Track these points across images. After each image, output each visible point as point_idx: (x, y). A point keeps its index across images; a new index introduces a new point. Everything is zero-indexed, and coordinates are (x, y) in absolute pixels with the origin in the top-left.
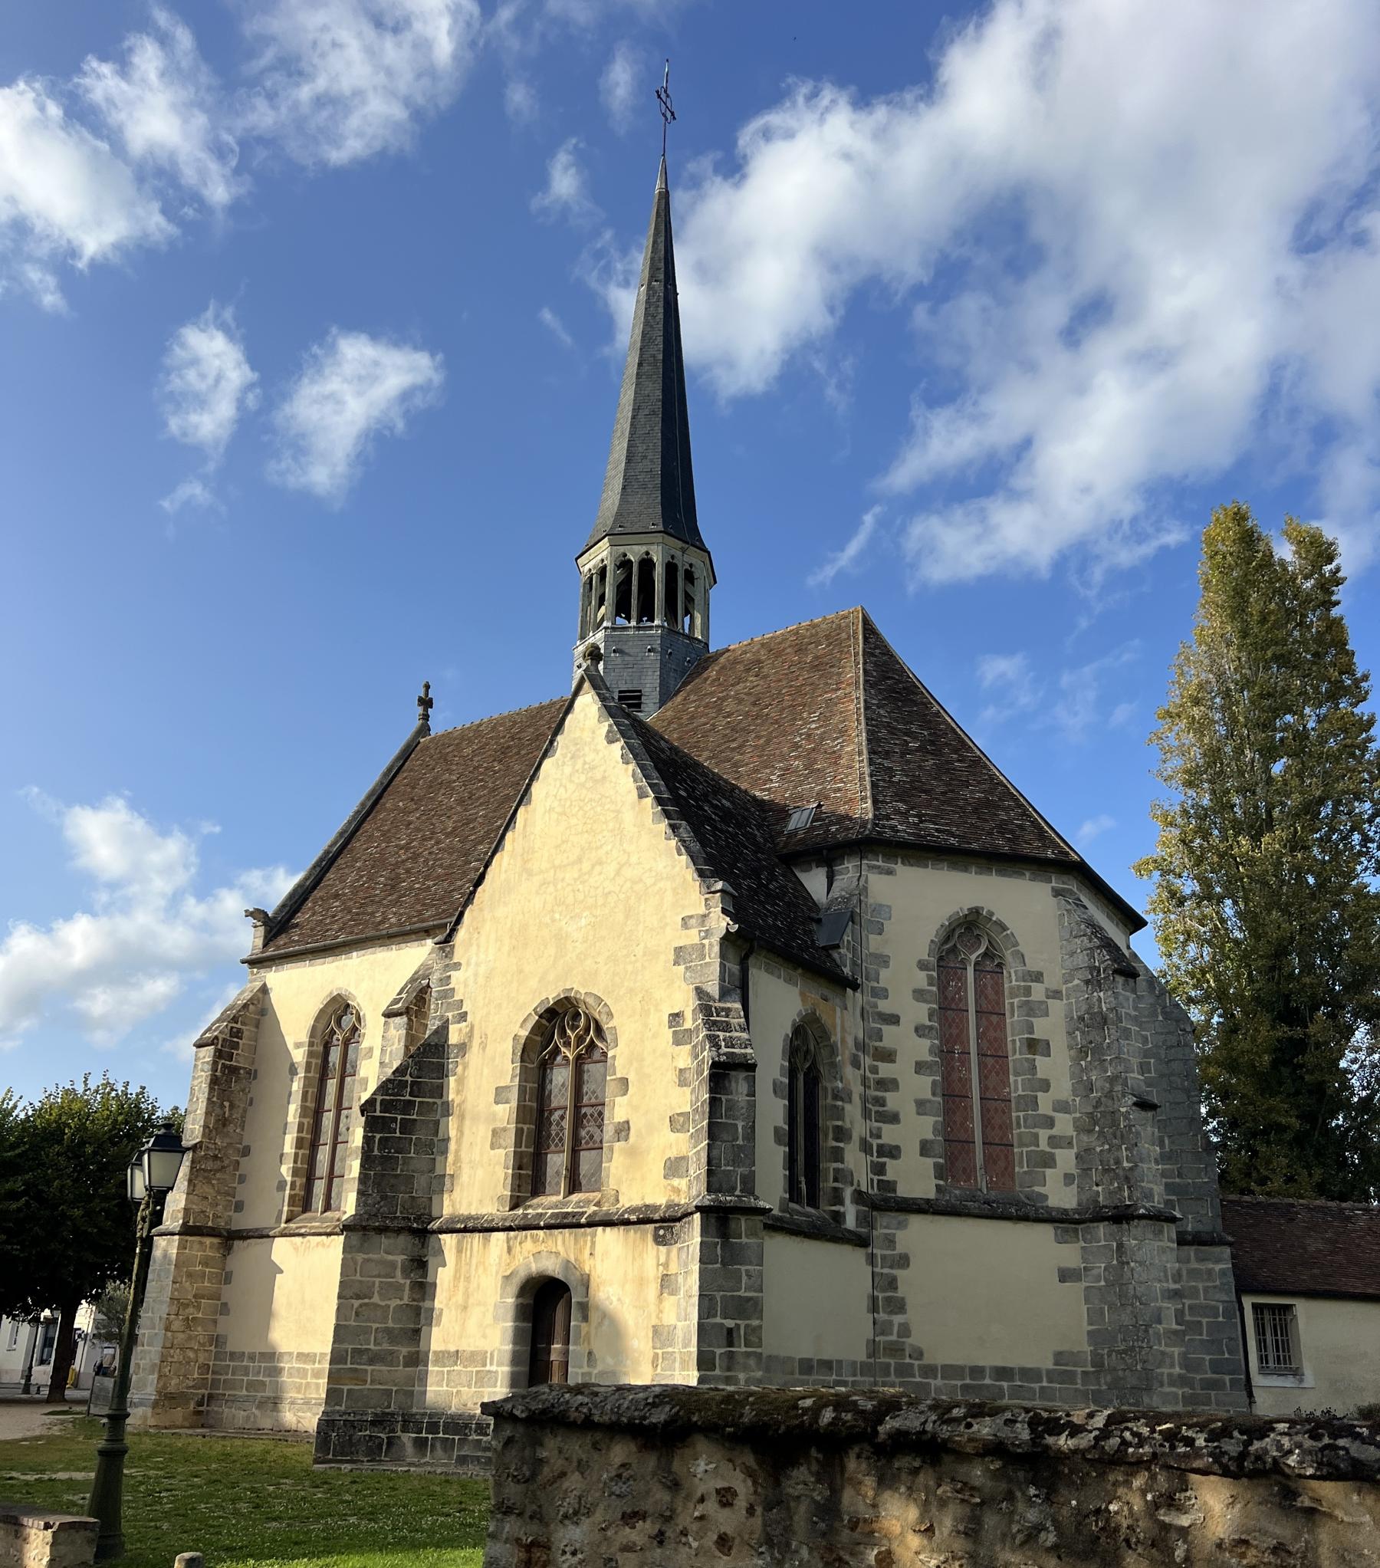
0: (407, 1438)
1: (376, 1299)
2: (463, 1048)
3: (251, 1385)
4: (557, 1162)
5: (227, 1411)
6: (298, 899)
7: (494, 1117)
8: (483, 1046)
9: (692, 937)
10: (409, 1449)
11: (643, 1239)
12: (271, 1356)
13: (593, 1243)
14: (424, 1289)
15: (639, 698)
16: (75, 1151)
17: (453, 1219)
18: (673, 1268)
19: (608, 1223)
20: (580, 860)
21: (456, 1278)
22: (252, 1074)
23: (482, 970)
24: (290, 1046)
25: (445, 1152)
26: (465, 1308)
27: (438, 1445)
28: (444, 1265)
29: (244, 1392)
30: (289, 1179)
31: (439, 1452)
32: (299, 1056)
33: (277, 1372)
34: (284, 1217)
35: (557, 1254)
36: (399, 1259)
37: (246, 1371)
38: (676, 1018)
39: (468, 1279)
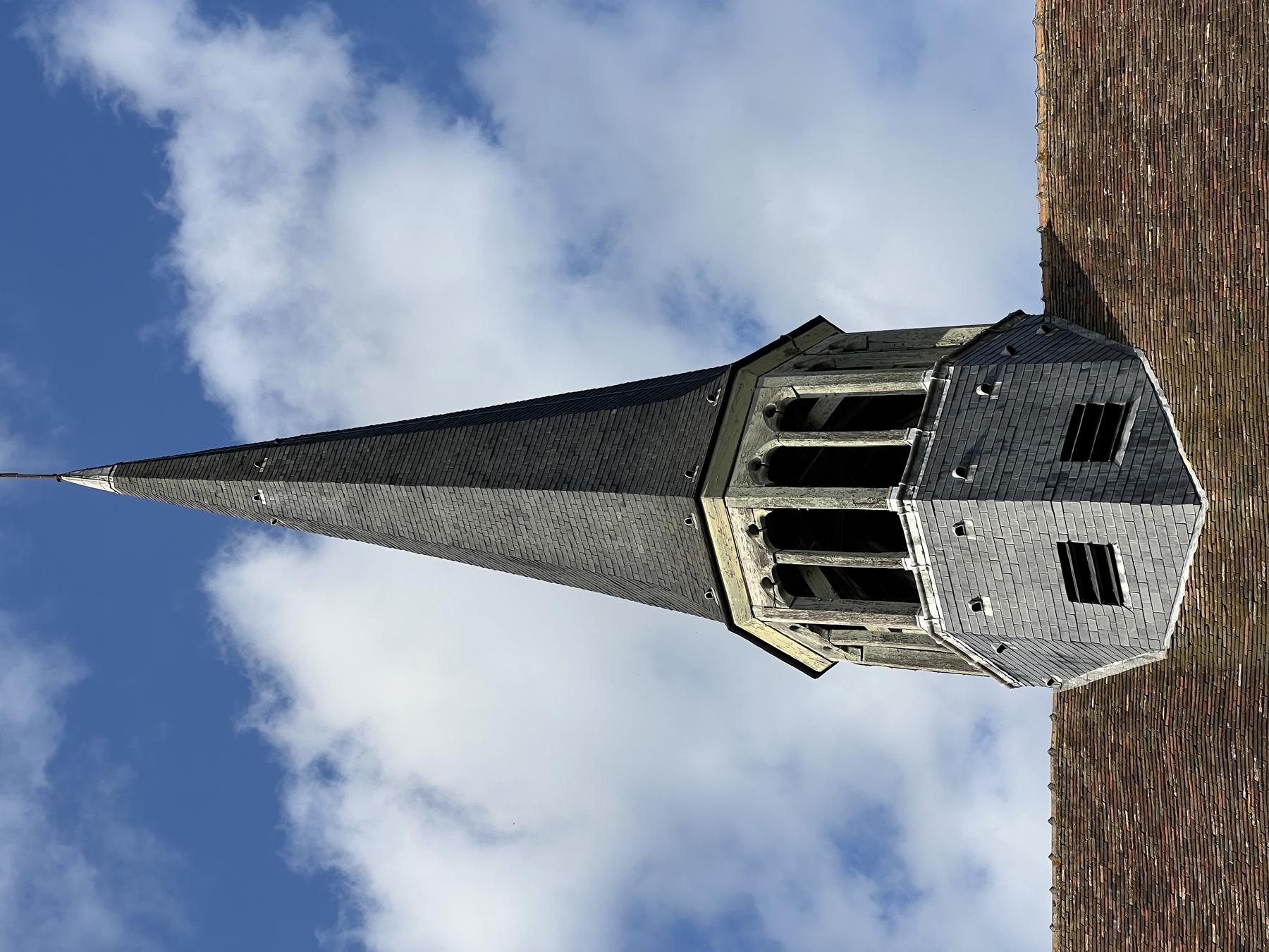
15: (1078, 549)
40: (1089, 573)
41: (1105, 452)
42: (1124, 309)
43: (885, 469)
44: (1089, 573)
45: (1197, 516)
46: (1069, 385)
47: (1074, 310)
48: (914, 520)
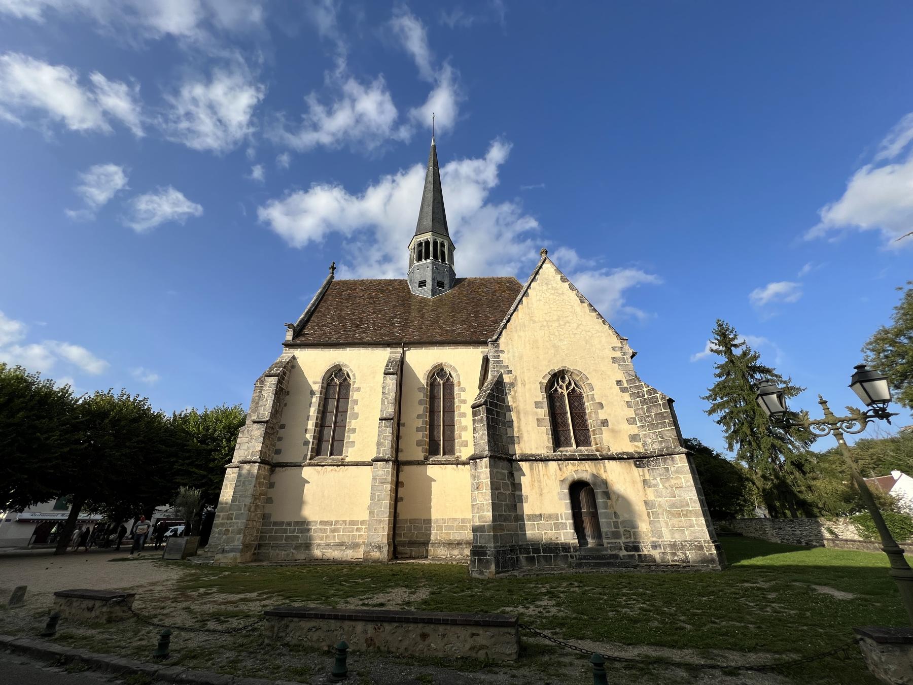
0: (522, 557)
1: (502, 490)
2: (512, 385)
3: (287, 538)
4: (327, 446)
5: (272, 552)
6: (304, 323)
7: (536, 414)
8: (524, 384)
9: (618, 354)
10: (523, 562)
11: (629, 463)
12: (304, 526)
13: (605, 467)
14: (517, 487)
16: (115, 422)
17: (522, 455)
18: (647, 477)
19: (611, 458)
20: (558, 320)
21: (533, 481)
22: (288, 393)
23: (517, 354)
24: (311, 383)
25: (512, 426)
26: (541, 495)
27: (542, 559)
28: (524, 475)
29: (284, 542)
30: (311, 440)
31: (543, 562)
32: (316, 388)
33: (309, 530)
34: (309, 457)
35: (587, 471)
36: (506, 472)
37: (285, 531)
38: (619, 382)
39: (539, 481)
40: (422, 284)
41: (438, 286)
42: (456, 288)
43: (436, 257)
44: (422, 284)
45: (430, 297)
46: (446, 281)
47: (456, 282)
48: (429, 261)
